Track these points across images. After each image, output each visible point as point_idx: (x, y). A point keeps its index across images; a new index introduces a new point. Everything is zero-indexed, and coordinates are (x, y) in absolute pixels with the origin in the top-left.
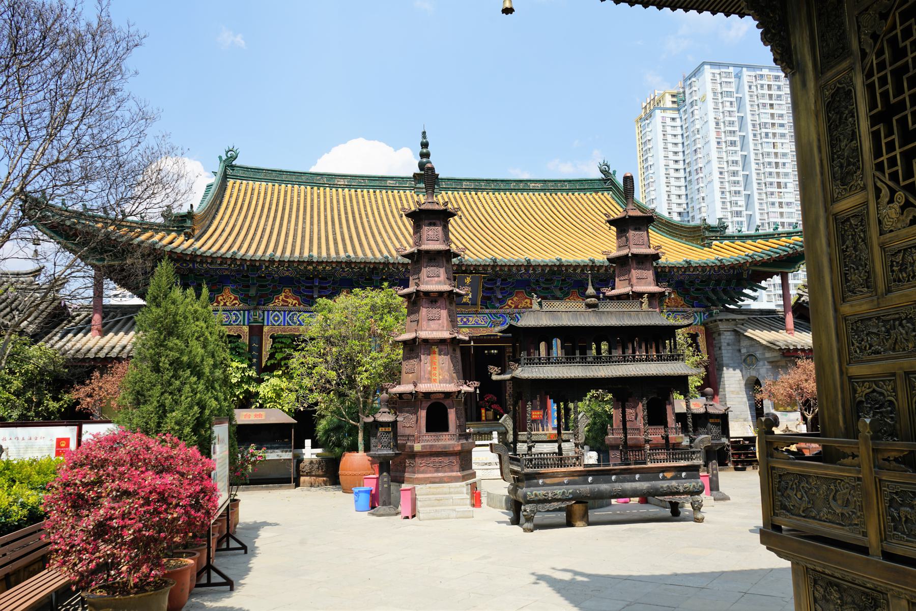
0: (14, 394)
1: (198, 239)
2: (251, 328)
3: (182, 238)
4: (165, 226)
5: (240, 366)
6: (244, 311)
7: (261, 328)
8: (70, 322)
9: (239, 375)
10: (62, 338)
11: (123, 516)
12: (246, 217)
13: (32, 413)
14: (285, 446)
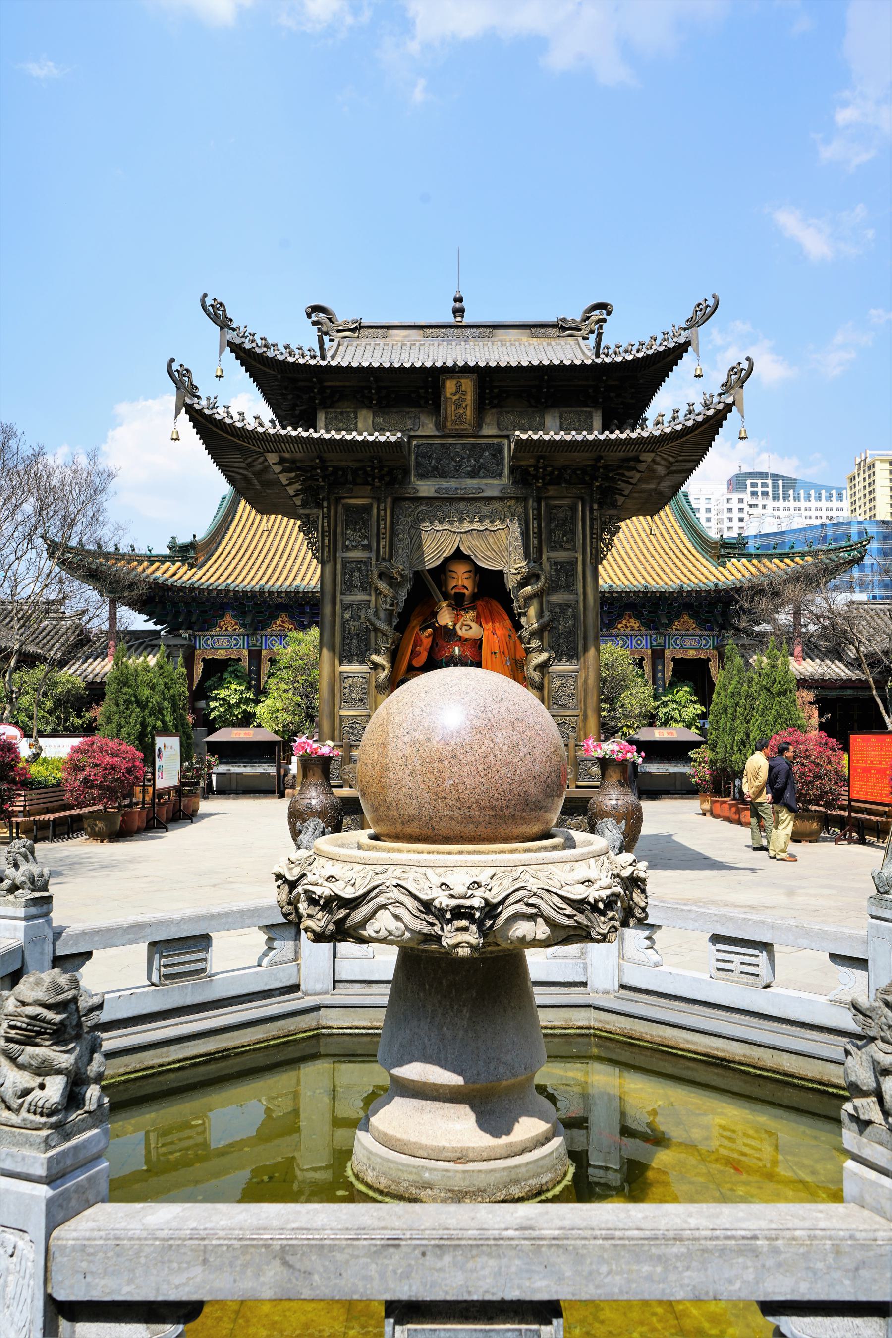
0: (48, 712)
1: (200, 568)
2: (250, 651)
3: (186, 567)
4: (170, 557)
5: (239, 688)
6: (244, 636)
7: (260, 651)
8: (91, 646)
9: (237, 697)
10: (83, 663)
11: (95, 775)
12: (254, 536)
13: (61, 728)
14: (270, 761)
